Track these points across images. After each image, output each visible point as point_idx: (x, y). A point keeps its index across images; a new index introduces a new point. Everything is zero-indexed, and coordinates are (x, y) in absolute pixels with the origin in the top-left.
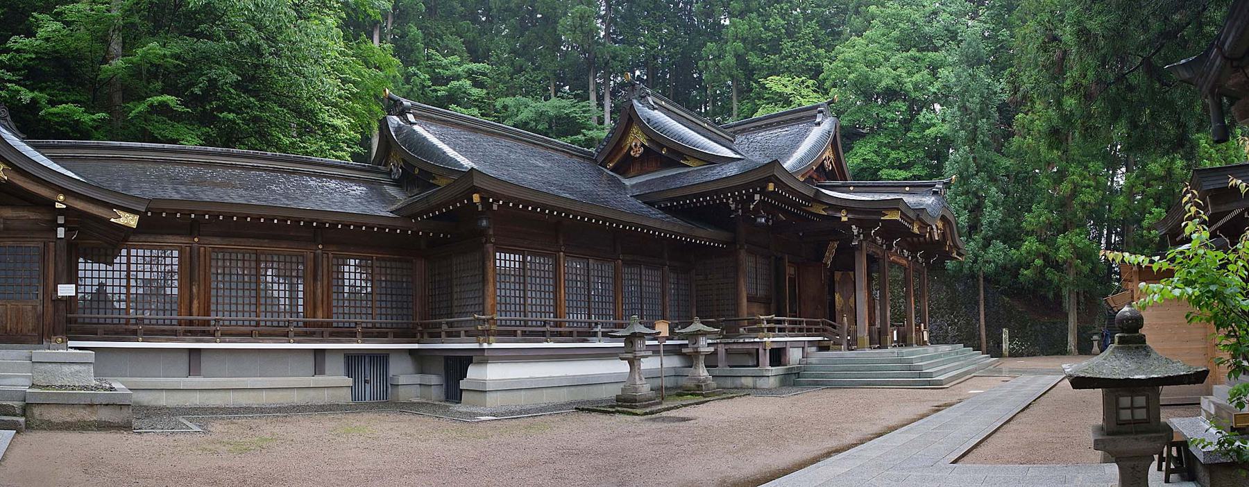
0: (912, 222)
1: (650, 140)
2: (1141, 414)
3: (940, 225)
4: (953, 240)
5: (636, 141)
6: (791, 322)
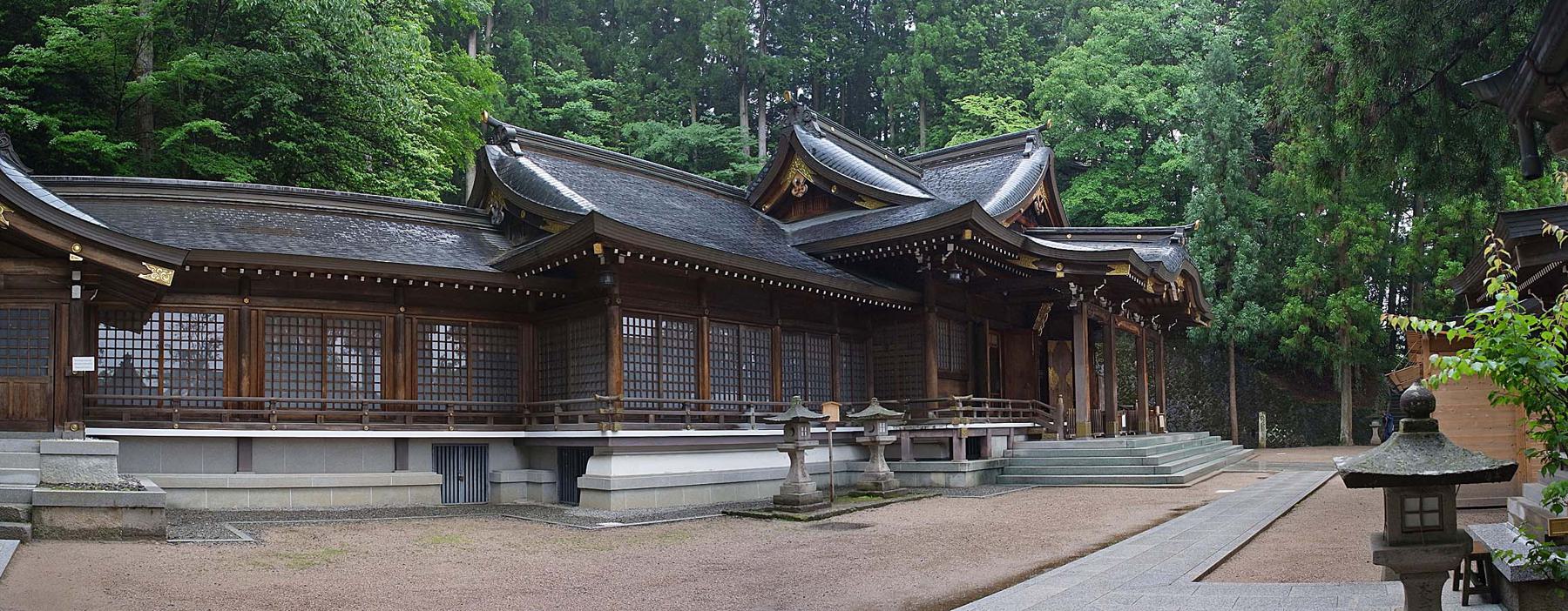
0: (1145, 279)
1: (816, 176)
2: (1432, 520)
3: (1180, 282)
4: (1197, 301)
5: (799, 177)
6: (993, 404)
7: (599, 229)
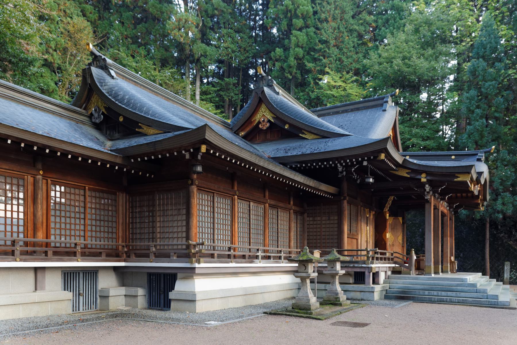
1: (276, 118)
5: (264, 116)
7: (208, 136)
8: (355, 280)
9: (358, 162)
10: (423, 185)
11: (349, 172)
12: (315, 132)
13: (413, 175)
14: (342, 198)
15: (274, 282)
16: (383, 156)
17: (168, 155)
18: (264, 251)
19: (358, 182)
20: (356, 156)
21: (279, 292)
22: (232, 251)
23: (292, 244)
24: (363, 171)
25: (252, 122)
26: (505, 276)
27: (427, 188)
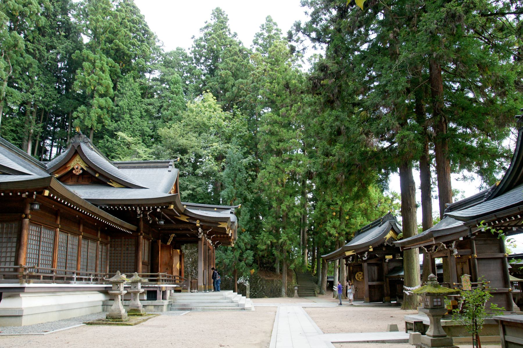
2: (439, 303)
5: (77, 165)
8: (148, 297)
9: (153, 209)
10: (197, 228)
11: (145, 215)
12: (121, 182)
13: (191, 221)
14: (139, 234)
15: (86, 298)
16: (172, 207)
17: (11, 194)
18: (77, 274)
19: (151, 222)
20: (153, 205)
21: (87, 309)
22: (54, 274)
23: (98, 269)
24: (155, 214)
25: (66, 168)
26: (247, 292)
27: (200, 230)
